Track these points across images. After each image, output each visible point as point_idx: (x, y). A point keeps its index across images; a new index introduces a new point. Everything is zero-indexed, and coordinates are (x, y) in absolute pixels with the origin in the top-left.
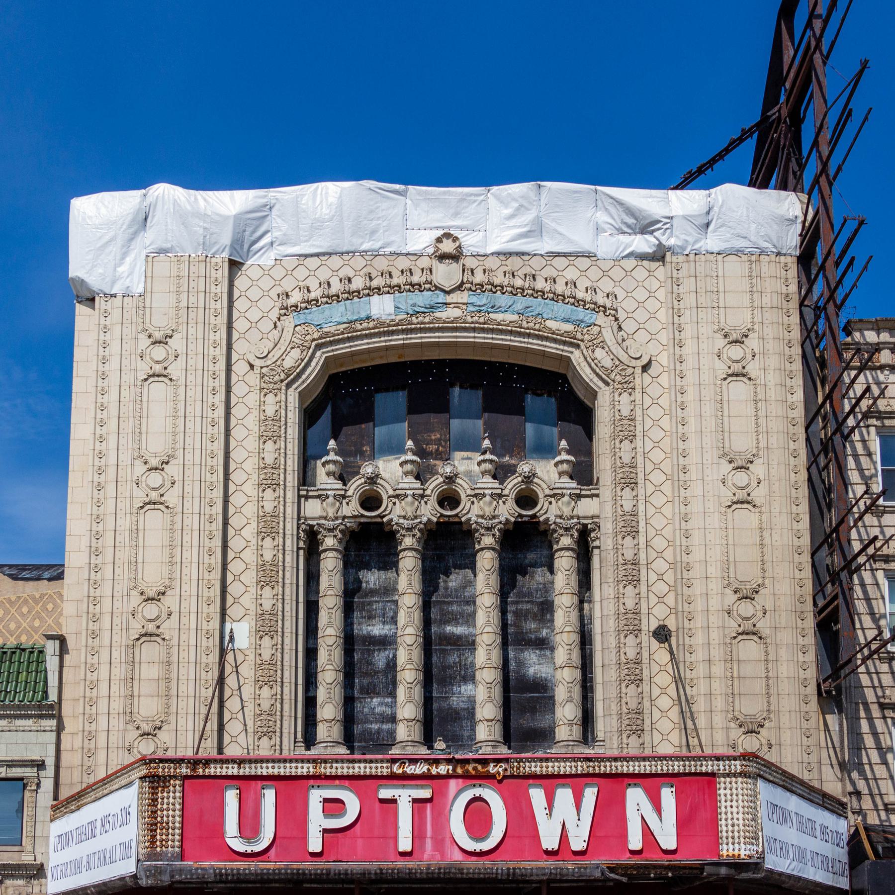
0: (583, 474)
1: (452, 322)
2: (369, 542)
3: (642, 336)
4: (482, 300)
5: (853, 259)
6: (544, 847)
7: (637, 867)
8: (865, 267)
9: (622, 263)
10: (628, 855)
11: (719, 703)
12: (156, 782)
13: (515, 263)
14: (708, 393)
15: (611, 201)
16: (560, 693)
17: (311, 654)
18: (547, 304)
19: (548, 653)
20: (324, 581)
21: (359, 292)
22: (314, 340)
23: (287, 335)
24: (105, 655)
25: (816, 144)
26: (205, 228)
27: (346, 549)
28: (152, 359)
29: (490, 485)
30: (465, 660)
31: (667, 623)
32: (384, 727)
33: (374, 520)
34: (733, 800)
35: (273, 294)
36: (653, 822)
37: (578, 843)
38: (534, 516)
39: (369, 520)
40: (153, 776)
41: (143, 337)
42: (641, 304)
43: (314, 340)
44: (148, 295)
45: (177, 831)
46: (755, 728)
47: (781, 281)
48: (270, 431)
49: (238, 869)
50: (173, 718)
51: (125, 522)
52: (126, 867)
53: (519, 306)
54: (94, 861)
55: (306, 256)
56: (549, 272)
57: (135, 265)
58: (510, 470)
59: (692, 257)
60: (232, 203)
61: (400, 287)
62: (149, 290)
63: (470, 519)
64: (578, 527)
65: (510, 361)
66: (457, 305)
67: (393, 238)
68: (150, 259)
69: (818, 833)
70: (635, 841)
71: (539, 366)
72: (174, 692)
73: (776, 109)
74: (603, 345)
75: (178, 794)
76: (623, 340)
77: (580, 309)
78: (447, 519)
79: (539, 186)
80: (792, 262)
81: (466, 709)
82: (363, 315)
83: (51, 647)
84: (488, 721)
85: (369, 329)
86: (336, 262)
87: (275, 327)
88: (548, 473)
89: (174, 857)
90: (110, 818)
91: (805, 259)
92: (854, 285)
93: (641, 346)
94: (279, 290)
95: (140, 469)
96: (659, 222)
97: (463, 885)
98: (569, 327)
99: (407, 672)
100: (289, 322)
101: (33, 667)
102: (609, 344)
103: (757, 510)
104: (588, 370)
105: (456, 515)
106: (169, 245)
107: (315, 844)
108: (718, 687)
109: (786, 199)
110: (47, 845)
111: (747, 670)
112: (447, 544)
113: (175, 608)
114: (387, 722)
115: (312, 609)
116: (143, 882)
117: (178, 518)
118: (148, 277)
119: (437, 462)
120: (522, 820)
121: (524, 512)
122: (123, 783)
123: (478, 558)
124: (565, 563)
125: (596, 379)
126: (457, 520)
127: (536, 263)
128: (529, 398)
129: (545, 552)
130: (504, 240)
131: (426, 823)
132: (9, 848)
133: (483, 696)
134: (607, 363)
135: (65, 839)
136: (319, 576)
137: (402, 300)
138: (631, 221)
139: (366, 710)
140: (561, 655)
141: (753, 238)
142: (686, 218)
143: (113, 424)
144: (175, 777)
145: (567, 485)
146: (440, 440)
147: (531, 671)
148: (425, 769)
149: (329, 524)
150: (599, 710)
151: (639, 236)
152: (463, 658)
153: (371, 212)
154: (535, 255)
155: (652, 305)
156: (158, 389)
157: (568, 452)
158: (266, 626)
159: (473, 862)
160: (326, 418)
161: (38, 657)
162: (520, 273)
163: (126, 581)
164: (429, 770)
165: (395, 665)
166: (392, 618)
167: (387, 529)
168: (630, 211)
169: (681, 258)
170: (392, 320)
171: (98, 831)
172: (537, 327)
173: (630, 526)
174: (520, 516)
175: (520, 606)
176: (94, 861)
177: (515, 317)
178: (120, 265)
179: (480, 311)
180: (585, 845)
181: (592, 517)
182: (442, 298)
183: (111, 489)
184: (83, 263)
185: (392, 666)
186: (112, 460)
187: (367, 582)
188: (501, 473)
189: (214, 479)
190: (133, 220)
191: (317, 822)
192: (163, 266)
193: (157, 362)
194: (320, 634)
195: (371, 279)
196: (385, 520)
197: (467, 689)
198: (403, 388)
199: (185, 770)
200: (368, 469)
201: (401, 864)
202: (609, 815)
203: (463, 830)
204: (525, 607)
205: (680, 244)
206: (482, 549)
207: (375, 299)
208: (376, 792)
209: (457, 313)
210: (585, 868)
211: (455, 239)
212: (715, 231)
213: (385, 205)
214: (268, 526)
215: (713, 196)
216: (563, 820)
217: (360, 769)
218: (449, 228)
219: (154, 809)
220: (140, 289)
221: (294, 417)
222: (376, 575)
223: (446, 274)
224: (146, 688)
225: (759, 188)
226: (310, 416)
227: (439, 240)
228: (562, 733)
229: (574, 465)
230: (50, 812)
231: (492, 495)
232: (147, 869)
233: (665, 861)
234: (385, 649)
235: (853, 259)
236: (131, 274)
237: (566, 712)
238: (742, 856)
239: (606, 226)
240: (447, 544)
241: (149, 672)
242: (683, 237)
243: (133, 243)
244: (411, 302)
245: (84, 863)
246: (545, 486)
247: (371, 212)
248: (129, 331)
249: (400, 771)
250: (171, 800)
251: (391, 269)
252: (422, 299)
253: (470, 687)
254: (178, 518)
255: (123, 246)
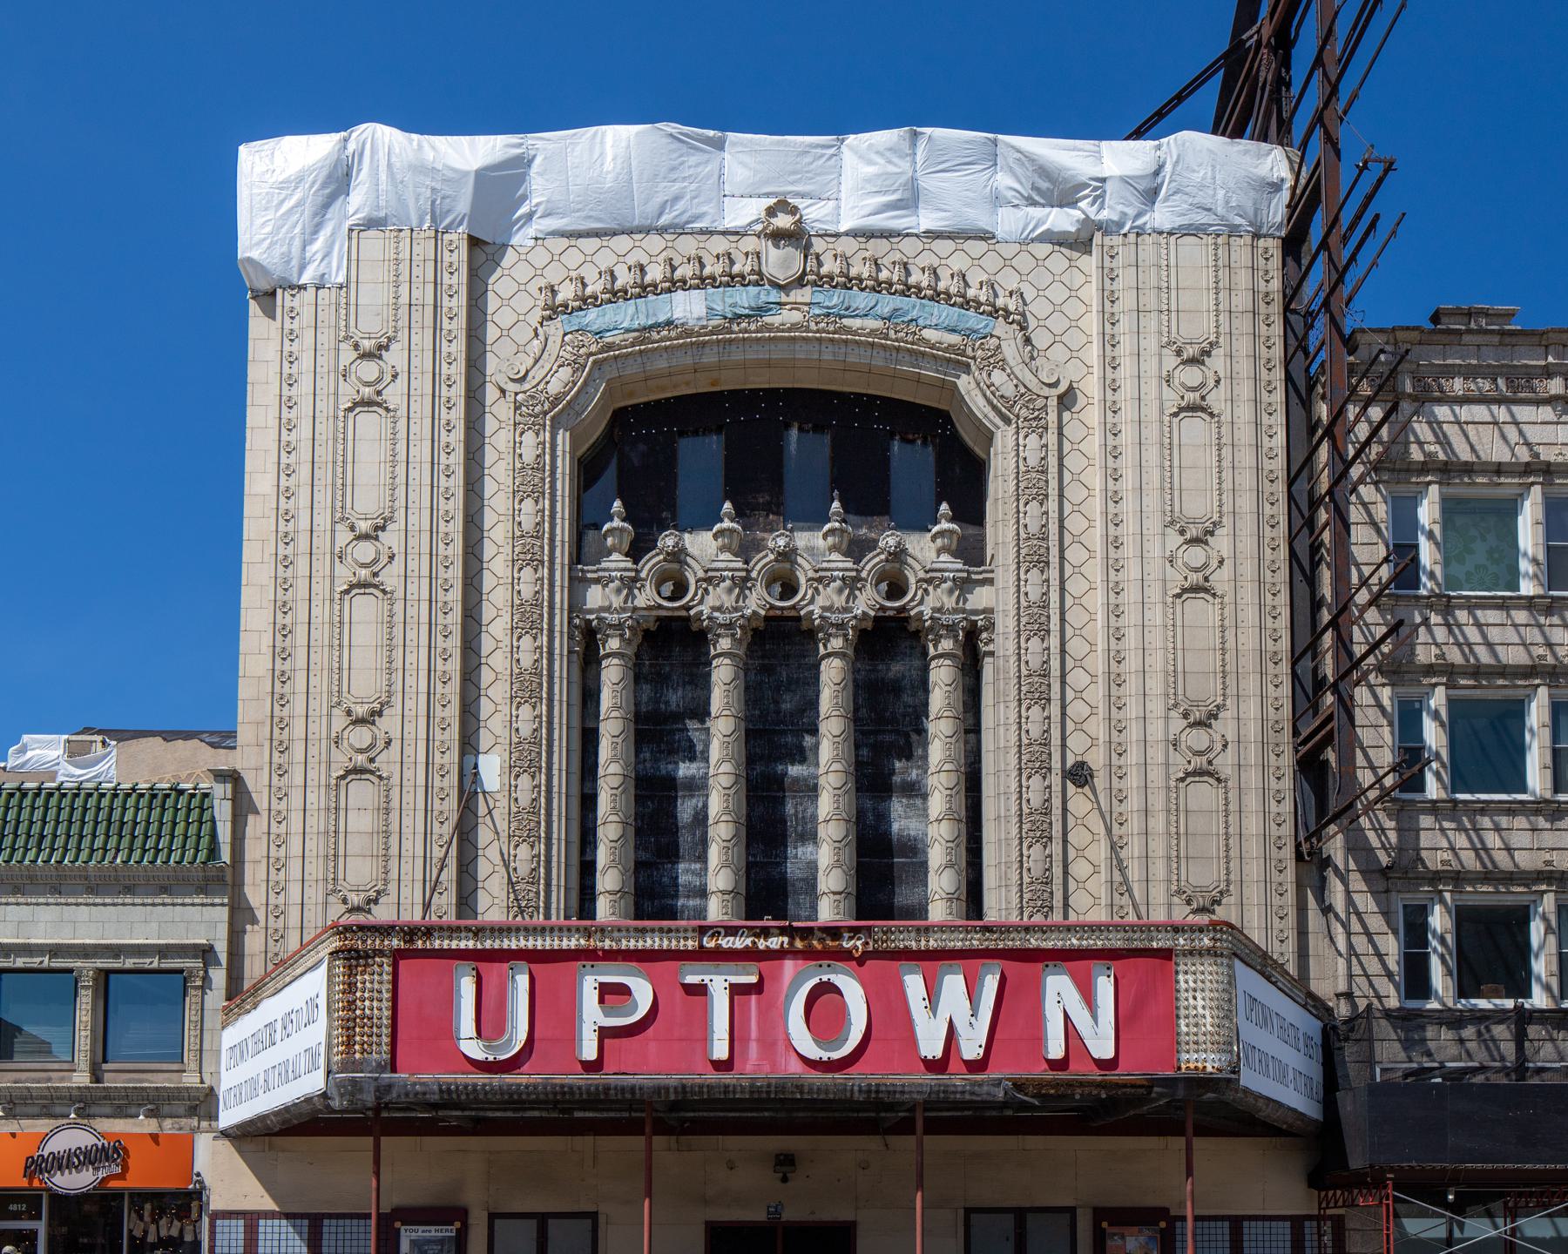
0: (972, 552)
1: (789, 330)
2: (671, 645)
3: (1058, 353)
4: (835, 298)
5: (1377, 217)
6: (923, 1054)
7: (1056, 1084)
8: (1394, 232)
9: (1032, 247)
10: (1045, 1066)
11: (1159, 870)
12: (352, 958)
13: (878, 247)
14: (1152, 433)
15: (1019, 155)
16: (936, 856)
17: (588, 802)
18: (924, 306)
19: (919, 802)
20: (607, 699)
21: (656, 286)
22: (591, 354)
23: (554, 347)
24: (296, 800)
25: (1319, 62)
26: (433, 189)
27: (637, 655)
28: (359, 379)
29: (840, 565)
30: (804, 811)
31: (1088, 758)
32: (691, 903)
33: (677, 614)
34: (1198, 992)
35: (533, 288)
36: (1080, 1018)
37: (971, 1048)
38: (903, 609)
39: (669, 614)
40: (349, 951)
41: (345, 347)
42: (1057, 308)
43: (591, 354)
44: (353, 286)
45: (385, 1031)
46: (1207, 904)
47: (1258, 272)
48: (532, 482)
49: (475, 1086)
50: (392, 887)
51: (321, 612)
52: (314, 1083)
53: (886, 310)
54: (274, 1078)
55: (580, 235)
56: (927, 259)
57: (333, 243)
58: (868, 546)
59: (1132, 237)
60: (471, 153)
61: (714, 279)
62: (353, 279)
63: (812, 612)
64: (964, 624)
65: (870, 392)
66: (796, 306)
67: (704, 209)
68: (354, 234)
69: (1301, 1045)
70: (1056, 1050)
71: (911, 399)
72: (394, 850)
73: (1255, 29)
74: (1002, 365)
75: (385, 977)
76: (1032, 358)
77: (971, 313)
78: (778, 613)
79: (915, 134)
80: (1274, 246)
81: (803, 880)
82: (662, 318)
83: (221, 791)
84: (834, 893)
85: (670, 339)
86: (622, 243)
87: (537, 335)
88: (925, 550)
89: (380, 1068)
90: (293, 1016)
91: (1292, 244)
92: (1374, 264)
93: (1057, 366)
94: (542, 283)
95: (344, 536)
96: (1086, 186)
97: (801, 1114)
98: (954, 339)
99: (722, 825)
100: (555, 328)
101: (194, 816)
102: (1012, 362)
103: (1218, 600)
104: (981, 401)
105: (793, 607)
106: (382, 214)
107: (589, 1051)
108: (1158, 847)
109: (1269, 154)
110: (218, 1063)
111: (1197, 823)
112: (780, 644)
113: (396, 734)
114: (695, 897)
115: (589, 739)
116: (336, 1103)
117: (399, 607)
118: (353, 261)
119: (765, 535)
120: (890, 1016)
121: (889, 604)
122: (309, 964)
123: (822, 667)
124: (942, 677)
125: (992, 414)
126: (793, 613)
127: (910, 246)
128: (896, 446)
129: (917, 663)
130: (863, 213)
131: (749, 1020)
132: (165, 1066)
133: (825, 861)
134: (1009, 390)
135: (240, 1051)
136: (599, 692)
137: (718, 298)
138: (1044, 185)
139: (665, 879)
140: (937, 804)
141: (1220, 211)
142: (1124, 180)
143: (305, 472)
144: (381, 953)
145: (950, 566)
146: (769, 503)
147: (895, 827)
148: (748, 941)
149: (613, 618)
150: (990, 878)
151: (1056, 210)
152: (800, 808)
153: (673, 169)
154: (908, 235)
155: (1074, 308)
156: (368, 422)
157: (952, 520)
158: (524, 760)
159: (815, 1076)
160: (610, 475)
161: (202, 802)
162: (886, 261)
163: (325, 696)
164: (754, 943)
165: (706, 817)
166: (702, 752)
167: (695, 627)
168: (1043, 171)
169: (1117, 240)
170: (704, 327)
171: (278, 1037)
172: (910, 338)
173: (1035, 621)
174: (883, 608)
175: (880, 738)
176: (274, 1078)
177: (878, 324)
178: (312, 241)
179: (828, 315)
180: (981, 1051)
181: (984, 611)
182: (774, 296)
183: (302, 565)
184: (260, 234)
185: (701, 818)
186: (304, 523)
187: (667, 703)
188: (857, 549)
189: (450, 552)
190: (329, 176)
191: (592, 1015)
192: (373, 243)
193: (367, 384)
194: (601, 772)
195: (673, 269)
196: (692, 612)
197: (803, 852)
198: (719, 430)
199: (396, 943)
200: (667, 541)
201: (713, 1077)
202: (1015, 1013)
203: (804, 1034)
204: (888, 738)
205: (1115, 218)
206: (829, 655)
207: (680, 295)
208: (676, 973)
209: (796, 317)
210: (980, 1085)
211: (794, 210)
212: (1166, 200)
213: (693, 160)
214: (527, 619)
215: (1164, 148)
216: (949, 1016)
217: (652, 942)
218: (785, 194)
219: (351, 997)
220: (341, 279)
221: (564, 466)
222: (680, 693)
223: (780, 262)
224: (355, 845)
225: (1232, 136)
226: (588, 471)
227: (771, 212)
228: (938, 912)
229: (962, 539)
230: (220, 1017)
231: (843, 579)
232: (340, 1085)
233: (1096, 1075)
234: (692, 796)
235: (1377, 217)
236: (327, 255)
237: (941, 882)
238: (1209, 1069)
239: (1010, 194)
240: (780, 644)
241: (360, 822)
242: (1120, 208)
243: (331, 210)
244: (729, 301)
245: (261, 1081)
246: (917, 567)
247: (673, 169)
248: (326, 338)
249: (712, 944)
250: (375, 980)
251: (701, 253)
252: (744, 298)
253: (810, 848)
254: (399, 607)
255: (315, 214)
